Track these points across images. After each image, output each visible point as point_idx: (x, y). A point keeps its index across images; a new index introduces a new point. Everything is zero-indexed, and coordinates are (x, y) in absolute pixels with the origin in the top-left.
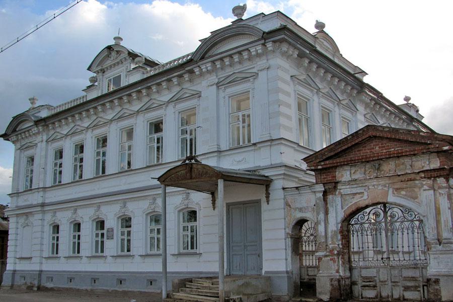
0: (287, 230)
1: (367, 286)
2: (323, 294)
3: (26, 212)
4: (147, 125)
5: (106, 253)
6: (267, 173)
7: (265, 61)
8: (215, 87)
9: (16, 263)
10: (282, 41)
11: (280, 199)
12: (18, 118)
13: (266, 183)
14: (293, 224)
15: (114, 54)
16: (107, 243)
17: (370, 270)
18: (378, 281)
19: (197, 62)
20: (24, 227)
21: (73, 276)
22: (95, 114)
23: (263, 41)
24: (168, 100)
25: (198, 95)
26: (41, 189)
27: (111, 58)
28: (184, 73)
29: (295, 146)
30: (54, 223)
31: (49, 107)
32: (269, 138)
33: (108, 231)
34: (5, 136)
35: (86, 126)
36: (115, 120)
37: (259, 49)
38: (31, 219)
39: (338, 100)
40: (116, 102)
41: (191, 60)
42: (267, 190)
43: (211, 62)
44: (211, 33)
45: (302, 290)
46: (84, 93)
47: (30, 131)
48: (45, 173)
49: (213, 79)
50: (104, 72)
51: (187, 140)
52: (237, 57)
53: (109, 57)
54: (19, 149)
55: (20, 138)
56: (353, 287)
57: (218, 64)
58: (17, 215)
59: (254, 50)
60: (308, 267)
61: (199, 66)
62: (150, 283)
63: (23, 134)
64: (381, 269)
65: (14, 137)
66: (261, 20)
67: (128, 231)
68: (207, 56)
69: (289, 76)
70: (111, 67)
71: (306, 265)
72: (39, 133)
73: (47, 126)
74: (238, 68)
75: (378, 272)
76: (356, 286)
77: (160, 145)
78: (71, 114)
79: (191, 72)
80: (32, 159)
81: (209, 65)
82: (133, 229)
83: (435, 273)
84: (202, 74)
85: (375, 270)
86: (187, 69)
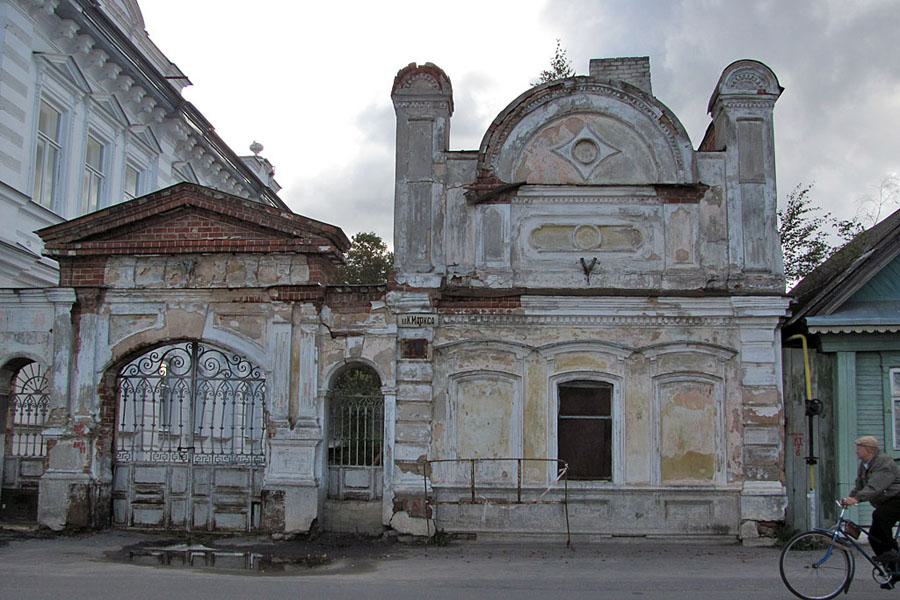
17: (155, 469)
18: (167, 492)
29: (23, 202)
39: (126, 124)
60: (22, 459)
64: (174, 469)
69: (30, 51)
71: (26, 455)
75: (169, 474)
76: (122, 502)
83: (278, 481)
85: (163, 471)
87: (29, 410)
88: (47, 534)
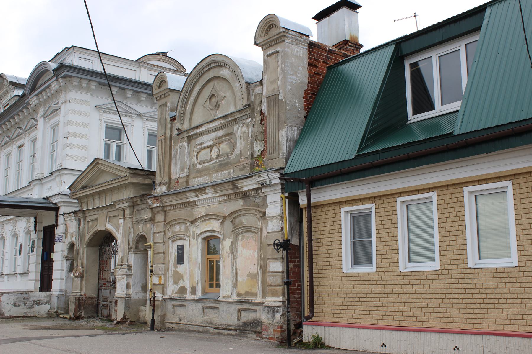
6: (55, 200)
13: (56, 209)
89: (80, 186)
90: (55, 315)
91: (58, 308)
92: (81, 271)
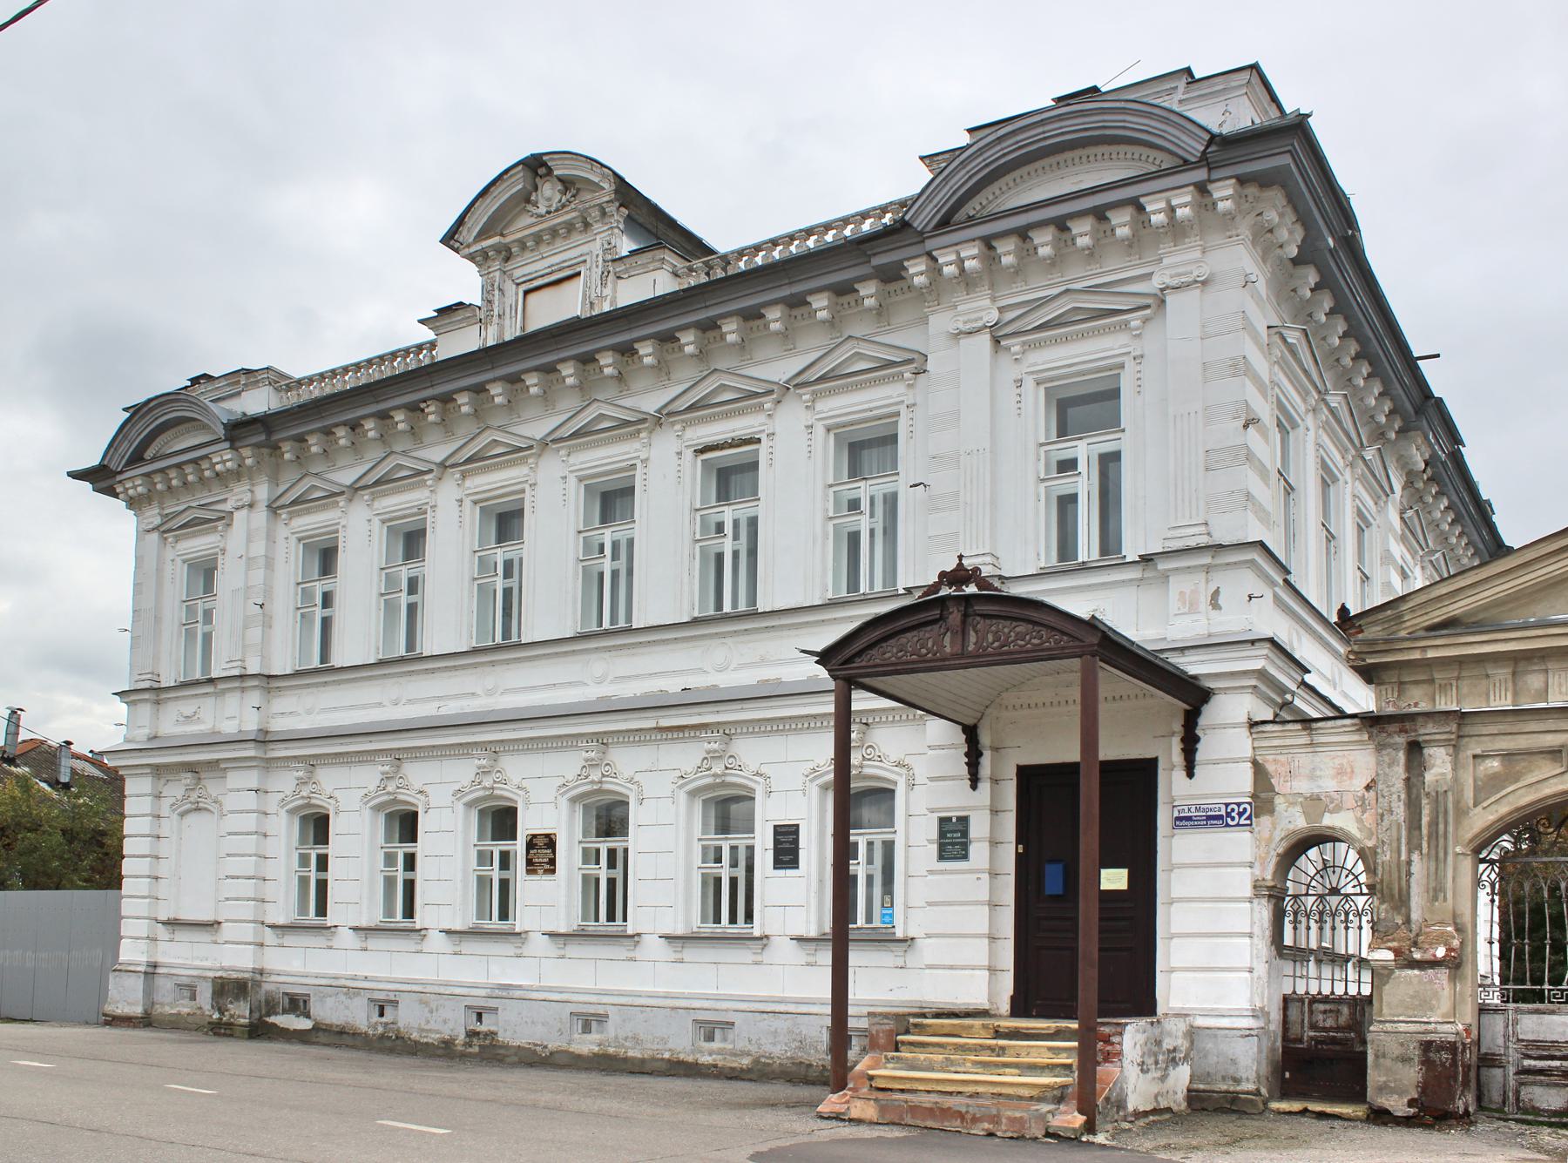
0: (1257, 871)
1: (1541, 1072)
2: (1393, 1091)
3: (193, 768)
4: (1036, 398)
5: (522, 919)
6: (1193, 665)
7: (1197, 254)
8: (985, 339)
9: (262, 945)
10: (1264, 181)
11: (1236, 761)
12: (151, 410)
14: (1280, 850)
15: (549, 192)
16: (528, 888)
17: (1554, 1017)
19: (922, 237)
20: (182, 815)
21: (492, 1003)
22: (581, 387)
23: (1200, 175)
24: (785, 378)
25: (917, 364)
26: (255, 683)
27: (535, 205)
28: (862, 279)
30: (395, 801)
31: (272, 378)
32: (1203, 540)
33: (531, 845)
34: (100, 477)
35: (438, 459)
36: (562, 440)
37: (1183, 203)
38: (212, 787)
40: (567, 370)
41: (902, 226)
42: (1191, 721)
43: (1195, 185)
44: (970, 131)
45: (1287, 1075)
46: (427, 334)
47: (205, 465)
48: (267, 624)
49: (982, 308)
50: (507, 259)
51: (601, 575)
52: (734, 326)
53: (528, 201)
54: (156, 528)
55: (159, 486)
56: (1484, 1071)
57: (1007, 252)
58: (158, 771)
59: (953, 257)
61: (929, 254)
62: (474, 1017)
63: (189, 469)
65: (139, 482)
66: (1179, 95)
67: (319, 856)
68: (961, 215)
70: (538, 239)
72: (237, 474)
73: (275, 448)
74: (1081, 276)
76: (1498, 1072)
77: (513, 583)
78: (318, 425)
79: (892, 275)
80: (205, 572)
81: (971, 251)
82: (638, 840)
84: (937, 286)
86: (876, 261)
87: (1321, 921)
88: (1380, 1117)
89: (1438, 616)
90: (1261, 1106)
91: (1258, 1077)
92: (1456, 943)
